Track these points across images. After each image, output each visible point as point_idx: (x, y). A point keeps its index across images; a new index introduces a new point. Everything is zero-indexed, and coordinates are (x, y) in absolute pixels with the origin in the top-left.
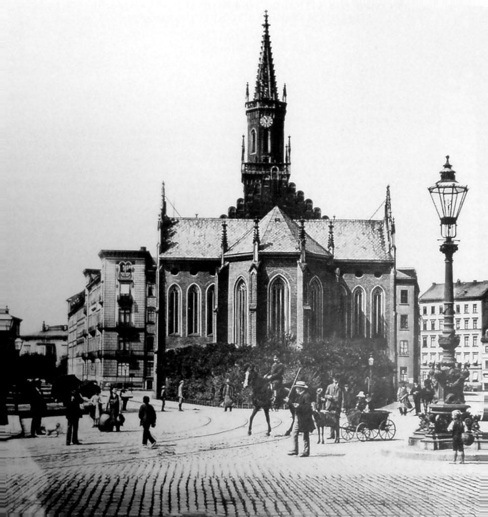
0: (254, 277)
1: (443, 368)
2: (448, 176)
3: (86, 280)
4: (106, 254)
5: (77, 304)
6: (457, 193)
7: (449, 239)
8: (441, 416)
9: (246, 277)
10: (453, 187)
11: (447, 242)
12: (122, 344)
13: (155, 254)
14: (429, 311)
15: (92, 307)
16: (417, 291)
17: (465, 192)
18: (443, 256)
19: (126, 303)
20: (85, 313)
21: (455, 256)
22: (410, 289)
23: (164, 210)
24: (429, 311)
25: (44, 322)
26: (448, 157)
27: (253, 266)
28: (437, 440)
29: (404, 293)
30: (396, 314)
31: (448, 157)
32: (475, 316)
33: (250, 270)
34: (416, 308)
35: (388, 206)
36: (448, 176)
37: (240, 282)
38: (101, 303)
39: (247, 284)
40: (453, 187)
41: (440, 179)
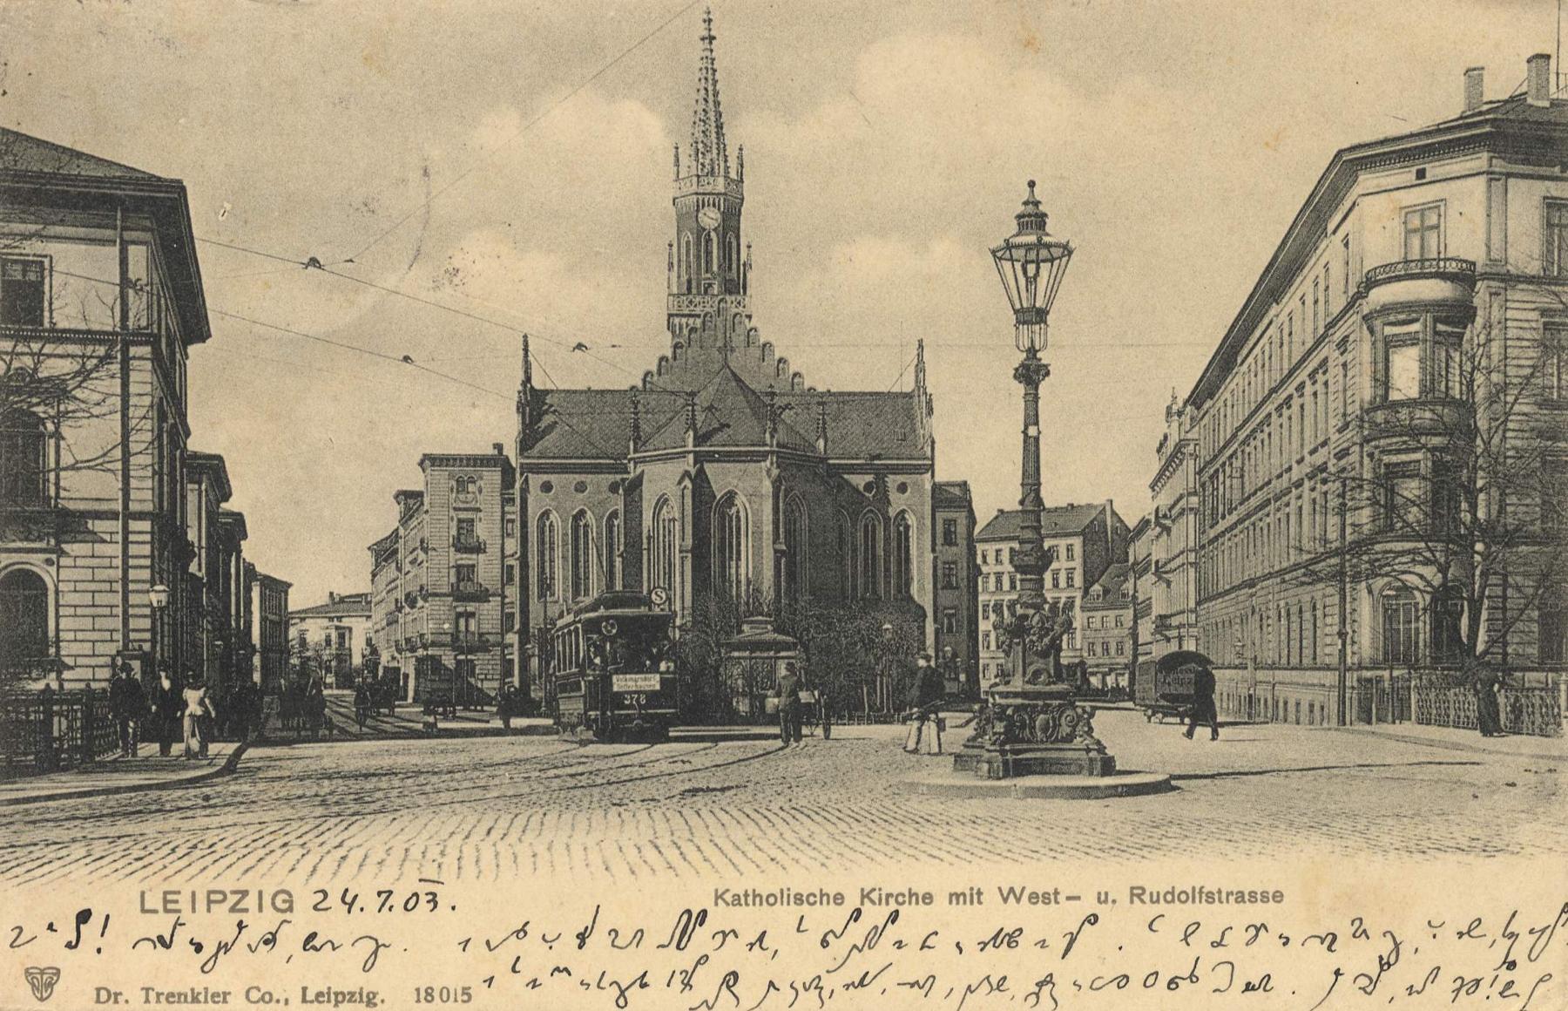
0: (688, 493)
1: (1019, 610)
2: (1033, 219)
3: (396, 510)
4: (431, 461)
5: (385, 552)
6: (1052, 260)
7: (1032, 352)
8: (1017, 708)
9: (672, 491)
10: (1040, 244)
11: (1028, 358)
12: (462, 621)
13: (511, 452)
14: (991, 559)
15: (410, 558)
16: (972, 521)
17: (1065, 259)
18: (1020, 389)
19: (466, 543)
20: (399, 569)
21: (1044, 388)
22: (961, 518)
23: (528, 379)
24: (991, 559)
25: (580, 947)
26: (1032, 184)
27: (687, 473)
28: (1009, 756)
29: (949, 523)
30: (935, 558)
31: (1032, 184)
32: (1071, 564)
33: (680, 483)
34: (972, 552)
35: (920, 368)
36: (1033, 219)
37: (662, 501)
38: (425, 550)
39: (674, 502)
40: (1040, 244)
41: (1014, 228)
